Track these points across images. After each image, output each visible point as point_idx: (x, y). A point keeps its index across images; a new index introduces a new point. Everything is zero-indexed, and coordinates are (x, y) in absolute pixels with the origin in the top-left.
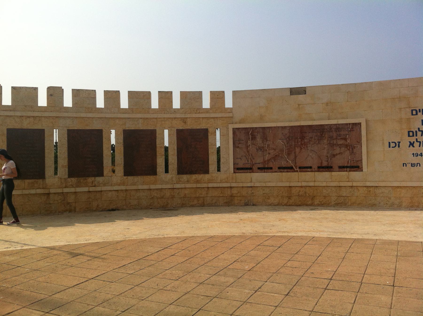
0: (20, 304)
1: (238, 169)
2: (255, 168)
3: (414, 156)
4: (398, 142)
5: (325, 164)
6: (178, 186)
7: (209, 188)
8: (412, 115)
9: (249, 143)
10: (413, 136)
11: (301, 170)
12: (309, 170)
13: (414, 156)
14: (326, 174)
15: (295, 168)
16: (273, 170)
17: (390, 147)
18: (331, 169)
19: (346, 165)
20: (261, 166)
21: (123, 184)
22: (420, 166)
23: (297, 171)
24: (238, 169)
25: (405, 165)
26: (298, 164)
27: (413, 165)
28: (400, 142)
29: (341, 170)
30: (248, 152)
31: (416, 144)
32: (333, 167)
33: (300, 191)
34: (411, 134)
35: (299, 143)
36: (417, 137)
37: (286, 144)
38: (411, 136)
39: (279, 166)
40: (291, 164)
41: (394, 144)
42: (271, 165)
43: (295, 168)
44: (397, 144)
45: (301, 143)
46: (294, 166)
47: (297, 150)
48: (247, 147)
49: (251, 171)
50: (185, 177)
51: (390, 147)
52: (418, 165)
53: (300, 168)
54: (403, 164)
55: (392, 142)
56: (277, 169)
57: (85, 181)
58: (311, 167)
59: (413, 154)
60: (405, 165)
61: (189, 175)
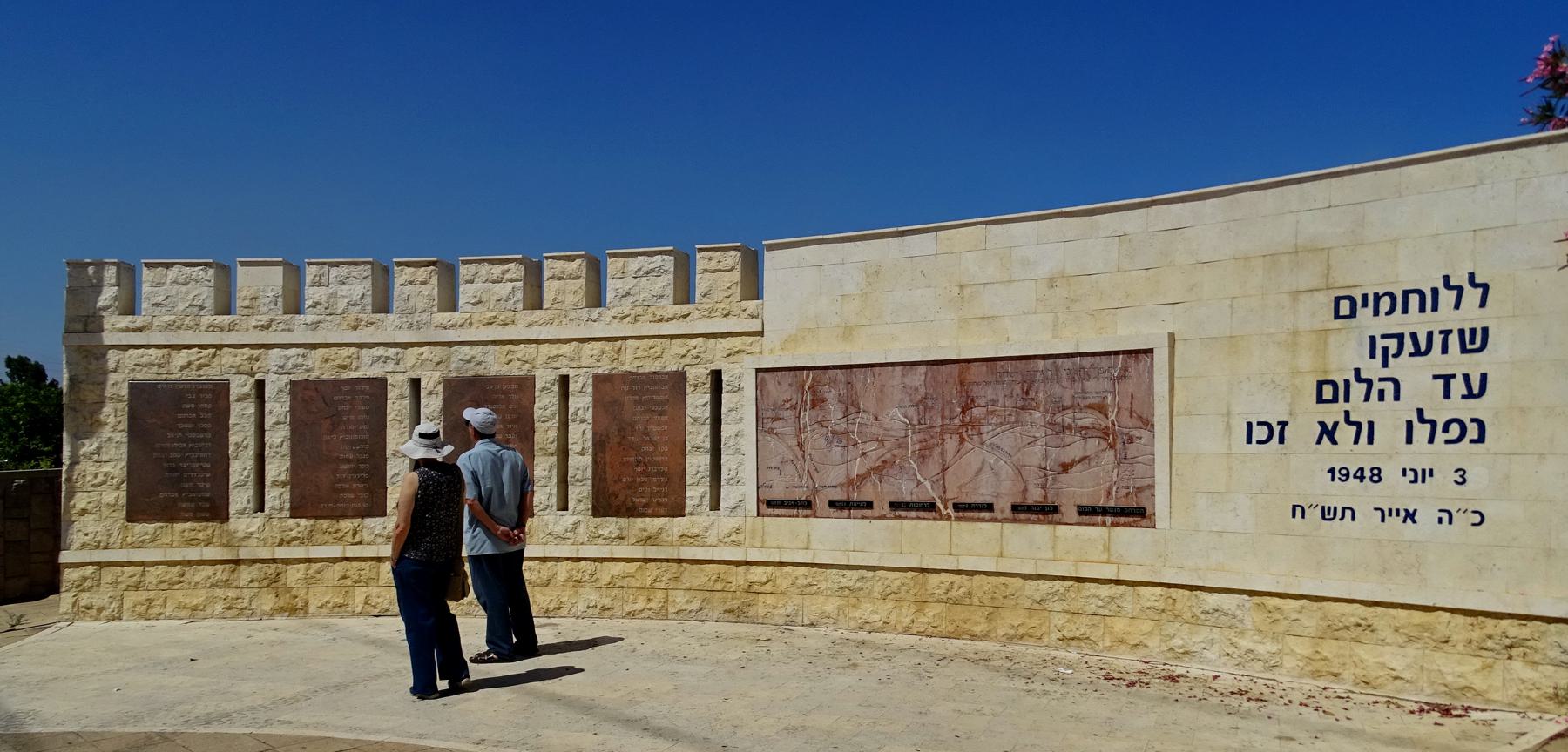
2: (821, 503)
4: (1279, 423)
5: (1035, 496)
8: (1337, 316)
10: (1335, 400)
13: (1333, 479)
14: (1039, 532)
15: (942, 507)
17: (1249, 441)
18: (1057, 517)
20: (839, 496)
22: (1353, 519)
23: (949, 518)
25: (1299, 511)
27: (1327, 514)
29: (1085, 518)
31: (1345, 433)
32: (1062, 509)
34: (1328, 391)
35: (957, 421)
36: (1347, 406)
39: (893, 498)
40: (929, 492)
42: (867, 494)
43: (942, 507)
44: (1277, 429)
45: (963, 421)
46: (940, 498)
47: (951, 443)
50: (612, 525)
52: (1348, 513)
53: (956, 507)
55: (1259, 423)
56: (887, 506)
59: (1332, 471)
60: (1299, 511)
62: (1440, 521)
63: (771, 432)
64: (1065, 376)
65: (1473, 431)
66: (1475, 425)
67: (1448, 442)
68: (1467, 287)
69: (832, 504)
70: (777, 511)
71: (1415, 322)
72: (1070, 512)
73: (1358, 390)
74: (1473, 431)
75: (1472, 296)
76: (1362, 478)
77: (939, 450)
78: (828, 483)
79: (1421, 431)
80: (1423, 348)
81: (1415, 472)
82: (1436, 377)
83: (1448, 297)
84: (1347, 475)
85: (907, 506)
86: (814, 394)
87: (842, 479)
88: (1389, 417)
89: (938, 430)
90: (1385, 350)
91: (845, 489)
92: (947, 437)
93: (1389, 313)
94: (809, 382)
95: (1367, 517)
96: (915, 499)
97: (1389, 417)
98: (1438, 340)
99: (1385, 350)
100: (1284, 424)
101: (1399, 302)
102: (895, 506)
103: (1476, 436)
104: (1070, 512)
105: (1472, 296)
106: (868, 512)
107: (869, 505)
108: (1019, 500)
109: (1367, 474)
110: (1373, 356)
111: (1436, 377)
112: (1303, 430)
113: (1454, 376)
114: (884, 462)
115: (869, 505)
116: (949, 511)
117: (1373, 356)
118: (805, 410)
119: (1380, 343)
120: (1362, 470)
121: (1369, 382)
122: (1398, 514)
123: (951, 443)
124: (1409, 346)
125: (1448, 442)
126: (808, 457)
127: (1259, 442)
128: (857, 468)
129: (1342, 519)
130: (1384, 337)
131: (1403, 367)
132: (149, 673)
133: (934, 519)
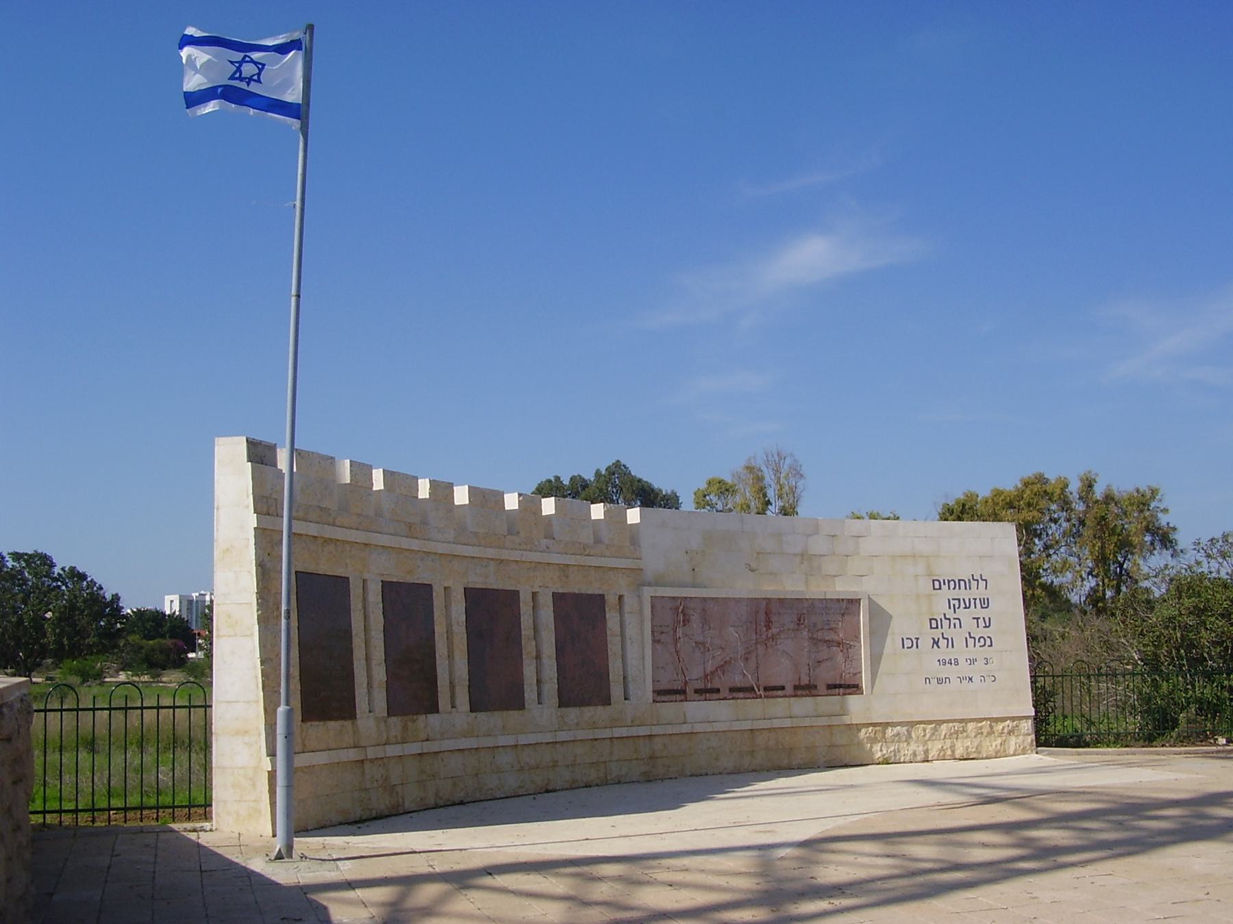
0: (140, 816)
1: (663, 693)
2: (689, 690)
3: (940, 664)
4: (916, 638)
6: (563, 736)
7: (613, 739)
8: (934, 589)
9: (680, 632)
10: (937, 627)
11: (767, 693)
12: (780, 693)
13: (940, 664)
15: (757, 690)
16: (721, 695)
17: (903, 647)
18: (814, 692)
19: (838, 683)
20: (700, 685)
21: (466, 734)
22: (950, 682)
24: (663, 693)
25: (928, 680)
26: (762, 683)
27: (940, 681)
28: (917, 639)
29: (830, 692)
30: (677, 652)
31: (943, 643)
32: (818, 687)
33: (769, 740)
34: (934, 623)
35: (764, 636)
36: (942, 631)
37: (742, 637)
38: (934, 628)
39: (731, 685)
40: (751, 680)
41: (910, 641)
43: (757, 690)
44: (915, 641)
45: (767, 636)
46: (756, 684)
47: (761, 649)
48: (676, 641)
49: (683, 697)
50: (572, 713)
51: (903, 647)
52: (947, 680)
53: (766, 689)
54: (926, 679)
55: (907, 639)
56: (727, 691)
57: (1040, 614)
58: (783, 688)
59: (939, 661)
60: (928, 680)
61: (578, 708)
62: (981, 681)
63: (659, 641)
64: (1153, 588)
65: (988, 643)
66: (989, 640)
67: (981, 646)
68: (980, 580)
69: (696, 691)
70: (664, 698)
71: (962, 594)
72: (822, 688)
73: (946, 623)
74: (988, 643)
75: (982, 584)
76: (951, 664)
77: (754, 654)
78: (694, 677)
79: (971, 641)
80: (968, 606)
81: (970, 660)
82: (974, 618)
83: (974, 584)
84: (945, 663)
85: (740, 690)
86: (684, 615)
87: (702, 674)
88: (958, 636)
89: (754, 642)
90: (954, 605)
91: (703, 681)
92: (759, 646)
93: (954, 589)
94: (681, 607)
95: (955, 682)
96: (743, 685)
97: (958, 636)
98: (972, 601)
99: (954, 605)
100: (917, 639)
101: (958, 583)
102: (732, 690)
103: (990, 644)
104: (822, 688)
105: (982, 584)
106: (715, 696)
107: (718, 691)
108: (797, 683)
109: (953, 662)
110: (950, 608)
111: (974, 618)
112: (926, 642)
113: (979, 618)
114: (725, 662)
115: (718, 691)
116: (761, 692)
117: (950, 608)
118: (679, 627)
119: (952, 602)
120: (951, 660)
121: (949, 619)
122: (966, 679)
123: (761, 649)
124: (963, 605)
125: (981, 646)
126: (681, 660)
127: (908, 648)
128: (710, 667)
129: (945, 682)
130: (953, 599)
131: (961, 612)
132: (524, 918)
133: (753, 698)
